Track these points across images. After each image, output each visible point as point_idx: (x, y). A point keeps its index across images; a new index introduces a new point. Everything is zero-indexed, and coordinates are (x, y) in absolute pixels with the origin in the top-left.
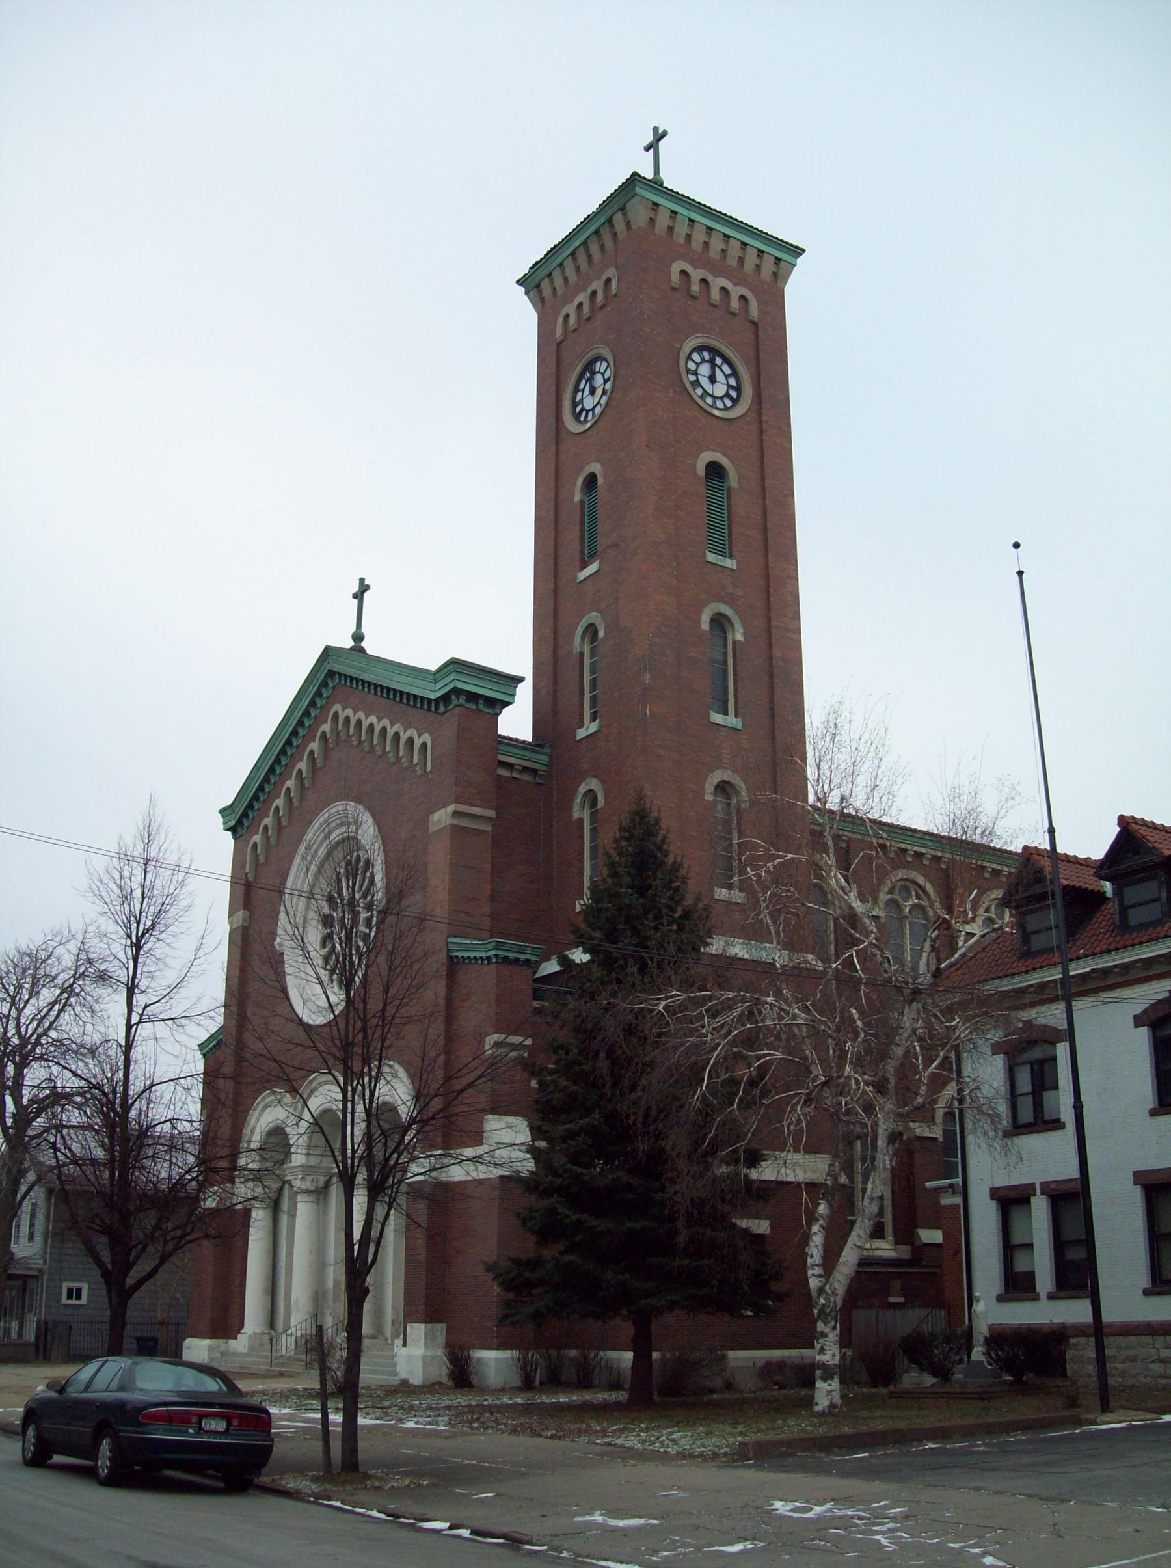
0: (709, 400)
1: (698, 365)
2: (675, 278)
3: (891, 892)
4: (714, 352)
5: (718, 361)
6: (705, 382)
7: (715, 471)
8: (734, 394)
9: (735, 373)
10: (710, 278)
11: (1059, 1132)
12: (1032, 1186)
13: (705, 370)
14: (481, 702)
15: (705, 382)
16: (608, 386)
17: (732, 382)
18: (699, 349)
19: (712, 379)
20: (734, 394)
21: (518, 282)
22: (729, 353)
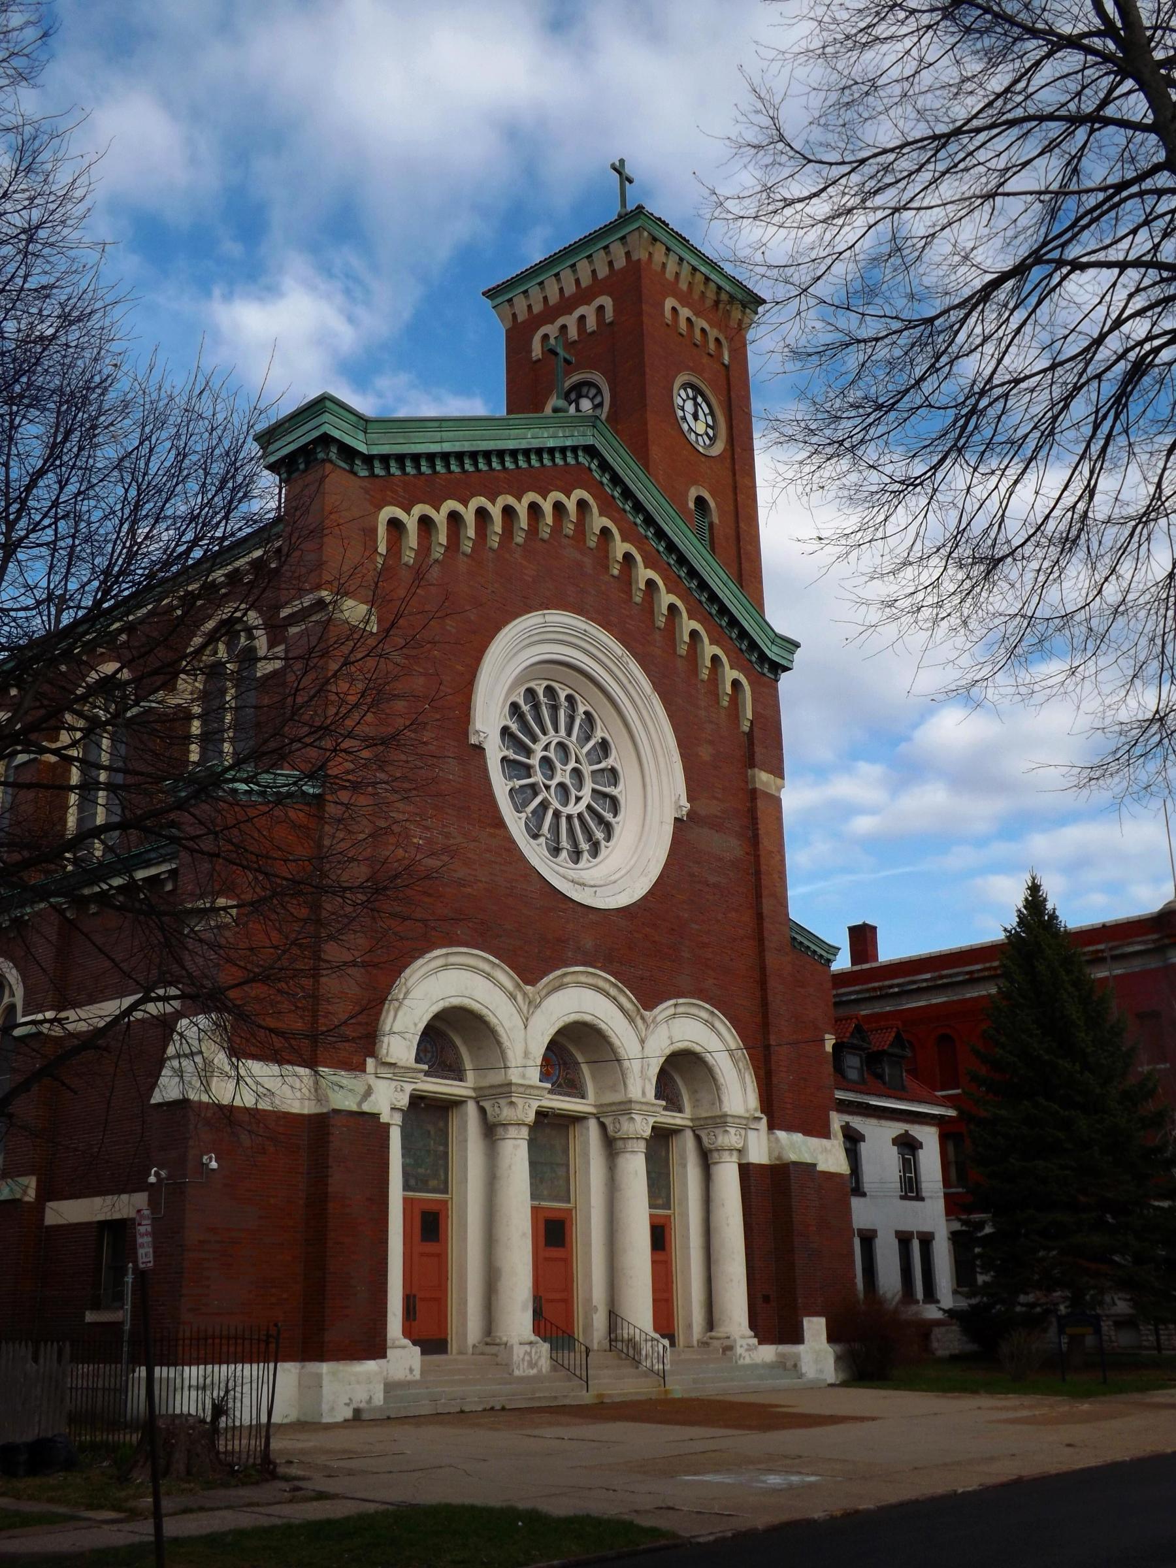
0: (693, 436)
1: (684, 401)
2: (668, 313)
3: (546, 748)
4: (698, 391)
5: (699, 400)
6: (690, 418)
7: (700, 501)
8: (710, 432)
9: (712, 413)
10: (679, 307)
11: (900, 1228)
12: (912, 1233)
13: (689, 406)
14: (334, 449)
15: (690, 418)
16: (685, 427)
17: (709, 419)
18: (685, 386)
19: (696, 417)
20: (710, 432)
21: (484, 294)
22: (708, 392)
